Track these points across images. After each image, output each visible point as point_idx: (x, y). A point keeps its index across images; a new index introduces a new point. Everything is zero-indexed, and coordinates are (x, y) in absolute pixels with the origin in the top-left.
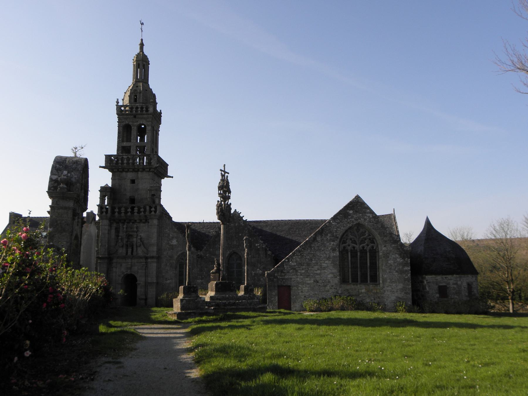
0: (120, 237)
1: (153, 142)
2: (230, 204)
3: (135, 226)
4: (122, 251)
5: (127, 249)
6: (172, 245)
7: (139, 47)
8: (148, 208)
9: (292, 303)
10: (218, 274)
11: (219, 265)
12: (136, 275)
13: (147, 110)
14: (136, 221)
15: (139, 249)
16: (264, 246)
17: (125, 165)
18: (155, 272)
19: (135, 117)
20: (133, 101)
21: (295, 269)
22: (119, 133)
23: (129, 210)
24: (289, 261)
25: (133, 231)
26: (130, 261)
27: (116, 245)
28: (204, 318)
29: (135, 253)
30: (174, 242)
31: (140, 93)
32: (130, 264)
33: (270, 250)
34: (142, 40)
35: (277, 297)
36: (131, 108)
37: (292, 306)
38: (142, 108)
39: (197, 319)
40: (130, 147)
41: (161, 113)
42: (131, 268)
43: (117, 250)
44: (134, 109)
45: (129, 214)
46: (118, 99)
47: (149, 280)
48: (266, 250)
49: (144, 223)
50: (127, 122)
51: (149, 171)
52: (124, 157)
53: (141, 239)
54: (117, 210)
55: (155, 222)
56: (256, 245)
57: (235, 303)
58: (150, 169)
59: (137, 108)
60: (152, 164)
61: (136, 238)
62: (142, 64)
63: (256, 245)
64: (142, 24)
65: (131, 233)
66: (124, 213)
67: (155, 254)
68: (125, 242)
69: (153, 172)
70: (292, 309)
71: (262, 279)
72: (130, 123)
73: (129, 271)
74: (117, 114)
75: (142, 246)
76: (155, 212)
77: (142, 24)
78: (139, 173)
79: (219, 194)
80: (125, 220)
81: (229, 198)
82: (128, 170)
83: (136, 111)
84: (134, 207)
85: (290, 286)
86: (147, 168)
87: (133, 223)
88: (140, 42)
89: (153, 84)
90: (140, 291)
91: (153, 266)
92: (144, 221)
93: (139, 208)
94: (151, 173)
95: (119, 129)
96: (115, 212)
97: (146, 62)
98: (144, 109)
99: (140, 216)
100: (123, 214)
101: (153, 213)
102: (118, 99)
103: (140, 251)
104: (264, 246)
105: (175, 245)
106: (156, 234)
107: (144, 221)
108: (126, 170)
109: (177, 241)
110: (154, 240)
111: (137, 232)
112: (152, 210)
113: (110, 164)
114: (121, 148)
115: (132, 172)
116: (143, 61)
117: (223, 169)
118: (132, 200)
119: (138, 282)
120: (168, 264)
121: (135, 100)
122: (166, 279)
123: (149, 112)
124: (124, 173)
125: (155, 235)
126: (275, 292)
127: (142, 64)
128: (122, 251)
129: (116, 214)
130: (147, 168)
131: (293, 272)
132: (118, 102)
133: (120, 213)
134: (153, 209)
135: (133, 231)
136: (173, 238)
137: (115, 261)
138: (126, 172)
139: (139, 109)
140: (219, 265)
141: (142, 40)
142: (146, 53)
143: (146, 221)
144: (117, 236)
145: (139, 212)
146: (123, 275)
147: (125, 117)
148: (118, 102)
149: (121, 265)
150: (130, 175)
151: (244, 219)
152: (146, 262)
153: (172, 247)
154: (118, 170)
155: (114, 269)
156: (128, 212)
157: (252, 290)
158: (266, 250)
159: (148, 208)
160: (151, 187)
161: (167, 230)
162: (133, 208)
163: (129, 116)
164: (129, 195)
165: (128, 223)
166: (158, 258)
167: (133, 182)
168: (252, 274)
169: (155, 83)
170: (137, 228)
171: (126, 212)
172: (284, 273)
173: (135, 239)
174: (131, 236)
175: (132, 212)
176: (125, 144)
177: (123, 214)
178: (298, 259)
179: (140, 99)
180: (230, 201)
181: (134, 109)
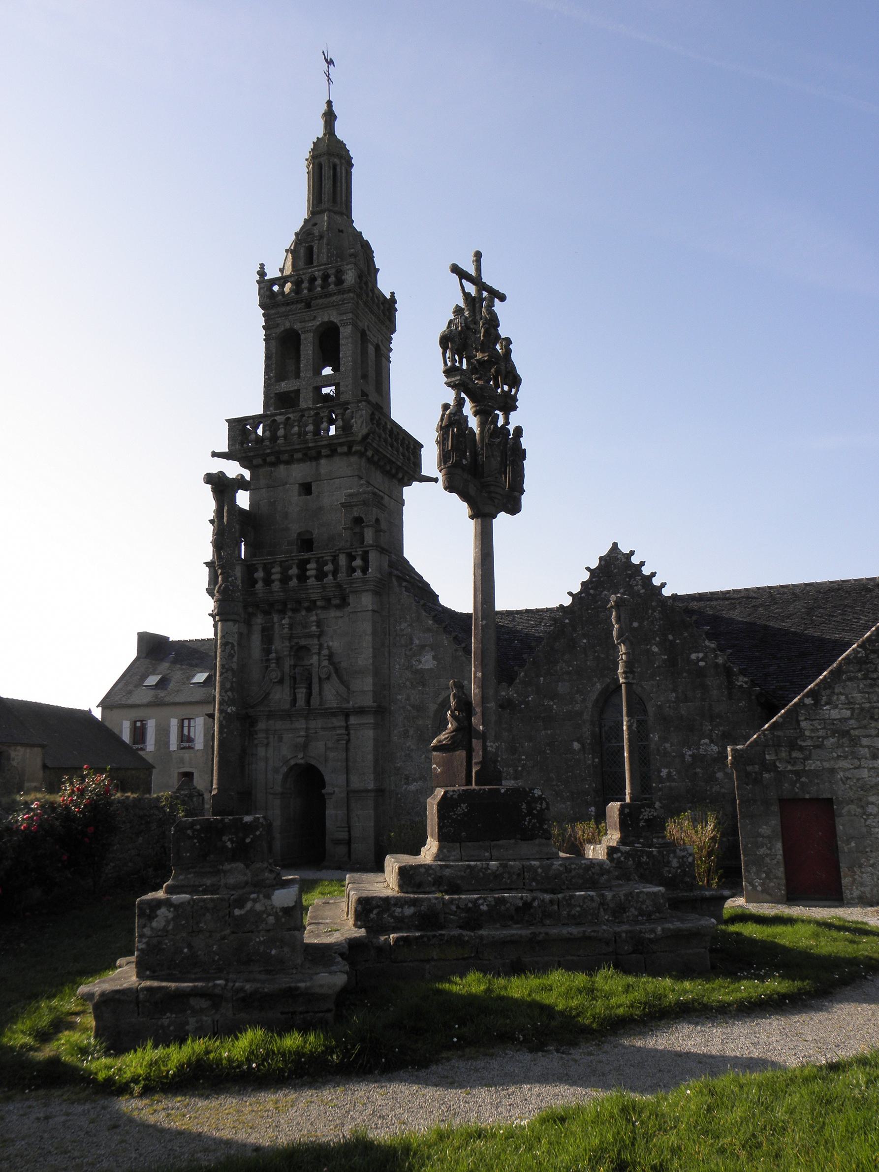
0: (273, 655)
1: (365, 377)
2: (519, 431)
3: (314, 618)
4: (280, 696)
5: (294, 688)
6: (421, 672)
7: (321, 123)
8: (343, 560)
9: (844, 869)
10: (461, 754)
11: (465, 706)
12: (321, 768)
13: (340, 282)
14: (315, 601)
15: (327, 687)
16: (720, 660)
17: (281, 441)
18: (370, 757)
19: (308, 306)
20: (301, 264)
21: (845, 733)
22: (268, 357)
23: (294, 571)
24: (817, 703)
25: (310, 636)
26: (301, 724)
27: (264, 677)
28: (242, 1045)
29: (315, 701)
30: (427, 661)
31: (321, 237)
32: (303, 733)
33: (743, 672)
34: (329, 103)
35: (779, 845)
36: (298, 284)
37: (846, 881)
38: (325, 277)
39: (176, 1056)
40: (297, 392)
41: (393, 300)
42: (305, 746)
43: (268, 694)
44: (305, 285)
45: (294, 582)
46: (262, 266)
47: (356, 783)
48: (728, 673)
49: (338, 607)
50: (288, 325)
51: (349, 453)
52: (277, 418)
53: (331, 657)
54: (260, 574)
55: (367, 601)
56: (694, 656)
57: (527, 905)
58: (350, 448)
59: (313, 280)
60: (355, 429)
61: (319, 654)
62: (331, 169)
63: (694, 656)
64: (330, 62)
65: (303, 642)
66: (281, 581)
67: (368, 701)
68: (287, 669)
69: (361, 454)
70: (847, 894)
71: (720, 775)
72: (297, 326)
73: (301, 755)
74: (262, 305)
75: (334, 676)
76: (365, 570)
77: (330, 62)
78: (323, 461)
79: (448, 372)
80: (285, 604)
81: (509, 404)
82: (319, 453)
83: (310, 290)
84: (308, 561)
85: (830, 801)
86: (341, 444)
87: (309, 610)
88: (324, 107)
89: (364, 219)
90: (333, 814)
91: (365, 737)
92: (336, 601)
93: (321, 563)
94: (354, 459)
95: (267, 348)
96: (256, 582)
97: (340, 157)
98: (332, 279)
99: (324, 587)
100: (276, 586)
101: (358, 574)
102: (262, 266)
103: (331, 694)
104: (720, 660)
105: (431, 670)
106: (369, 638)
107: (336, 601)
108: (286, 457)
109: (434, 658)
110: (364, 658)
111: (319, 637)
112: (354, 564)
113: (242, 443)
114: (277, 397)
115: (300, 461)
116: (329, 154)
117: (472, 271)
118: (306, 543)
119: (328, 789)
120: (411, 732)
121: (310, 260)
122: (407, 778)
123: (345, 285)
124: (282, 467)
125: (367, 643)
126: (770, 827)
127: (331, 169)
128: (280, 696)
129: (260, 585)
130: (341, 444)
131: (839, 746)
132: (262, 273)
133: (268, 582)
134: (358, 562)
135: (310, 636)
136: (422, 647)
137: (261, 725)
138: (288, 463)
139: (319, 282)
140: (465, 706)
141: (329, 103)
142: (341, 133)
143: (344, 602)
144: (267, 651)
145: (321, 575)
146: (285, 769)
147: (283, 309)
148: (262, 273)
149: (281, 739)
150: (298, 472)
151: (666, 592)
152: (347, 728)
153: (421, 678)
154: (264, 460)
155: (261, 752)
156: (290, 578)
157: (657, 825)
158: (728, 673)
159: (343, 560)
160: (351, 495)
161: (404, 625)
162: (303, 565)
163: (293, 307)
164: (295, 528)
165: (295, 611)
166: (380, 711)
167: (306, 489)
168: (683, 756)
169: (366, 217)
170: (319, 624)
171: (285, 579)
172: (801, 749)
173: (315, 658)
174: (306, 649)
175: (303, 577)
176: (284, 386)
177: (276, 586)
178: (858, 696)
179: (322, 255)
180: (515, 419)
181: (305, 285)
